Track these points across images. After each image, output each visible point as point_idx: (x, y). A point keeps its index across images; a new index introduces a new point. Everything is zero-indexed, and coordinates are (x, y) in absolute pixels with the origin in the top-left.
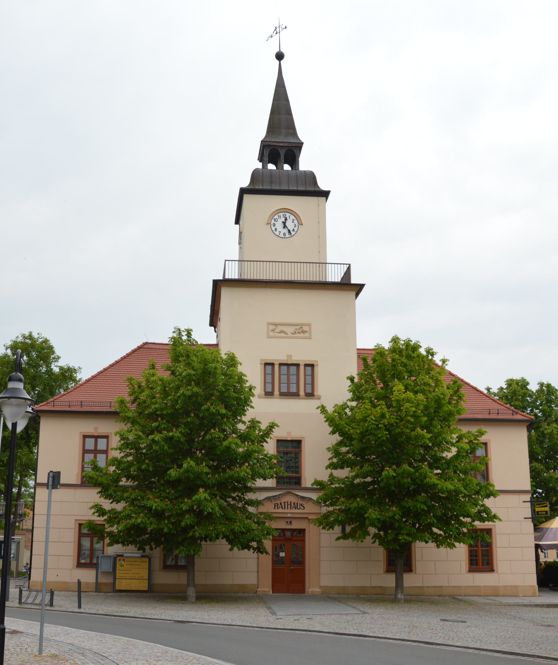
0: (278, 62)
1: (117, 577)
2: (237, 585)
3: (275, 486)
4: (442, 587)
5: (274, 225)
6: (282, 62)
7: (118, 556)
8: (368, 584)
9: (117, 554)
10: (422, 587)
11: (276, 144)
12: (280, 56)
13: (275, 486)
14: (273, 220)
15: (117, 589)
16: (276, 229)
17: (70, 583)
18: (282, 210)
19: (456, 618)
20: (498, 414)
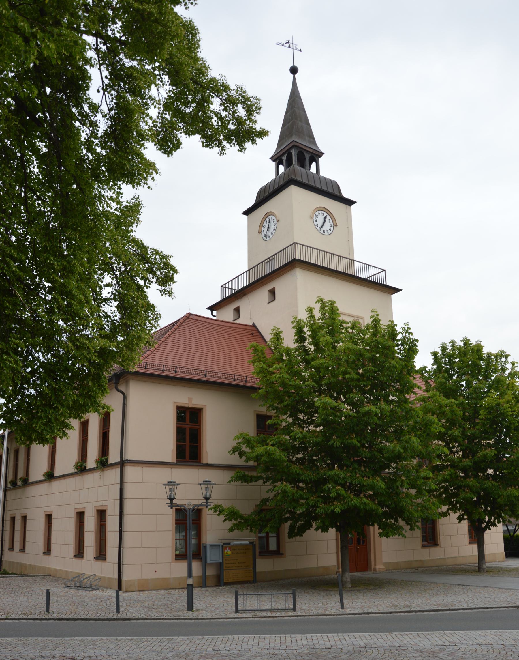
0: (292, 75)
1: (224, 568)
2: (321, 567)
3: (175, 462)
4: (456, 557)
5: (316, 221)
6: (296, 75)
7: (224, 544)
8: (412, 559)
9: (223, 541)
10: (444, 559)
11: (303, 147)
12: (294, 70)
13: (175, 462)
14: (315, 216)
15: (225, 581)
16: (317, 225)
17: (169, 579)
18: (322, 209)
19: (157, 615)
20: (163, 371)
